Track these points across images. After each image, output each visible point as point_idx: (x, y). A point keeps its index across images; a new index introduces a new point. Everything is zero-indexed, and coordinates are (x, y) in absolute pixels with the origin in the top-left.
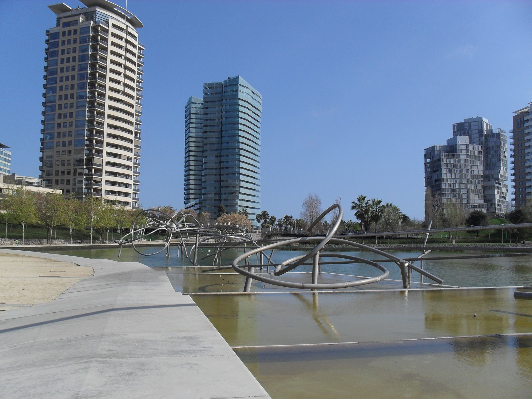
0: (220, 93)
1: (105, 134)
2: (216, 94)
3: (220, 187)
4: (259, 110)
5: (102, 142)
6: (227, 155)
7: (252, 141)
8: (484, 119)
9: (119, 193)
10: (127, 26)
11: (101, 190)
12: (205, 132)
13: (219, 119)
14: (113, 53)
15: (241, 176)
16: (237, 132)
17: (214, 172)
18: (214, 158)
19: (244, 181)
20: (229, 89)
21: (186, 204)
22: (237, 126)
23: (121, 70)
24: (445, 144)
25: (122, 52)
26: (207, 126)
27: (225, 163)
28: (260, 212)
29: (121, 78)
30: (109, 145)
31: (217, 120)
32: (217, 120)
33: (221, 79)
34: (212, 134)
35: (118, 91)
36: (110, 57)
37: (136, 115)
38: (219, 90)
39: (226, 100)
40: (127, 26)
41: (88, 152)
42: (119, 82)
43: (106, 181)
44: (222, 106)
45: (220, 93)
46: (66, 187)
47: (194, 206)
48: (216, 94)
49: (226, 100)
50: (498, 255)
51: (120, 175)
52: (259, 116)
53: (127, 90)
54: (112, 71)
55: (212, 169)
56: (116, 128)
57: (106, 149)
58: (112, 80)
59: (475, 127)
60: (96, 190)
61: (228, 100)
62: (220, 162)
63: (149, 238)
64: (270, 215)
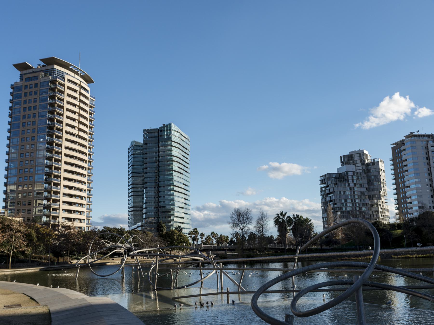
6: (164, 186)
10: (80, 81)
13: (156, 153)
24: (348, 154)
27: (162, 188)
30: (65, 179)
36: (67, 106)
38: (156, 134)
40: (80, 81)
48: (154, 137)
56: (72, 164)
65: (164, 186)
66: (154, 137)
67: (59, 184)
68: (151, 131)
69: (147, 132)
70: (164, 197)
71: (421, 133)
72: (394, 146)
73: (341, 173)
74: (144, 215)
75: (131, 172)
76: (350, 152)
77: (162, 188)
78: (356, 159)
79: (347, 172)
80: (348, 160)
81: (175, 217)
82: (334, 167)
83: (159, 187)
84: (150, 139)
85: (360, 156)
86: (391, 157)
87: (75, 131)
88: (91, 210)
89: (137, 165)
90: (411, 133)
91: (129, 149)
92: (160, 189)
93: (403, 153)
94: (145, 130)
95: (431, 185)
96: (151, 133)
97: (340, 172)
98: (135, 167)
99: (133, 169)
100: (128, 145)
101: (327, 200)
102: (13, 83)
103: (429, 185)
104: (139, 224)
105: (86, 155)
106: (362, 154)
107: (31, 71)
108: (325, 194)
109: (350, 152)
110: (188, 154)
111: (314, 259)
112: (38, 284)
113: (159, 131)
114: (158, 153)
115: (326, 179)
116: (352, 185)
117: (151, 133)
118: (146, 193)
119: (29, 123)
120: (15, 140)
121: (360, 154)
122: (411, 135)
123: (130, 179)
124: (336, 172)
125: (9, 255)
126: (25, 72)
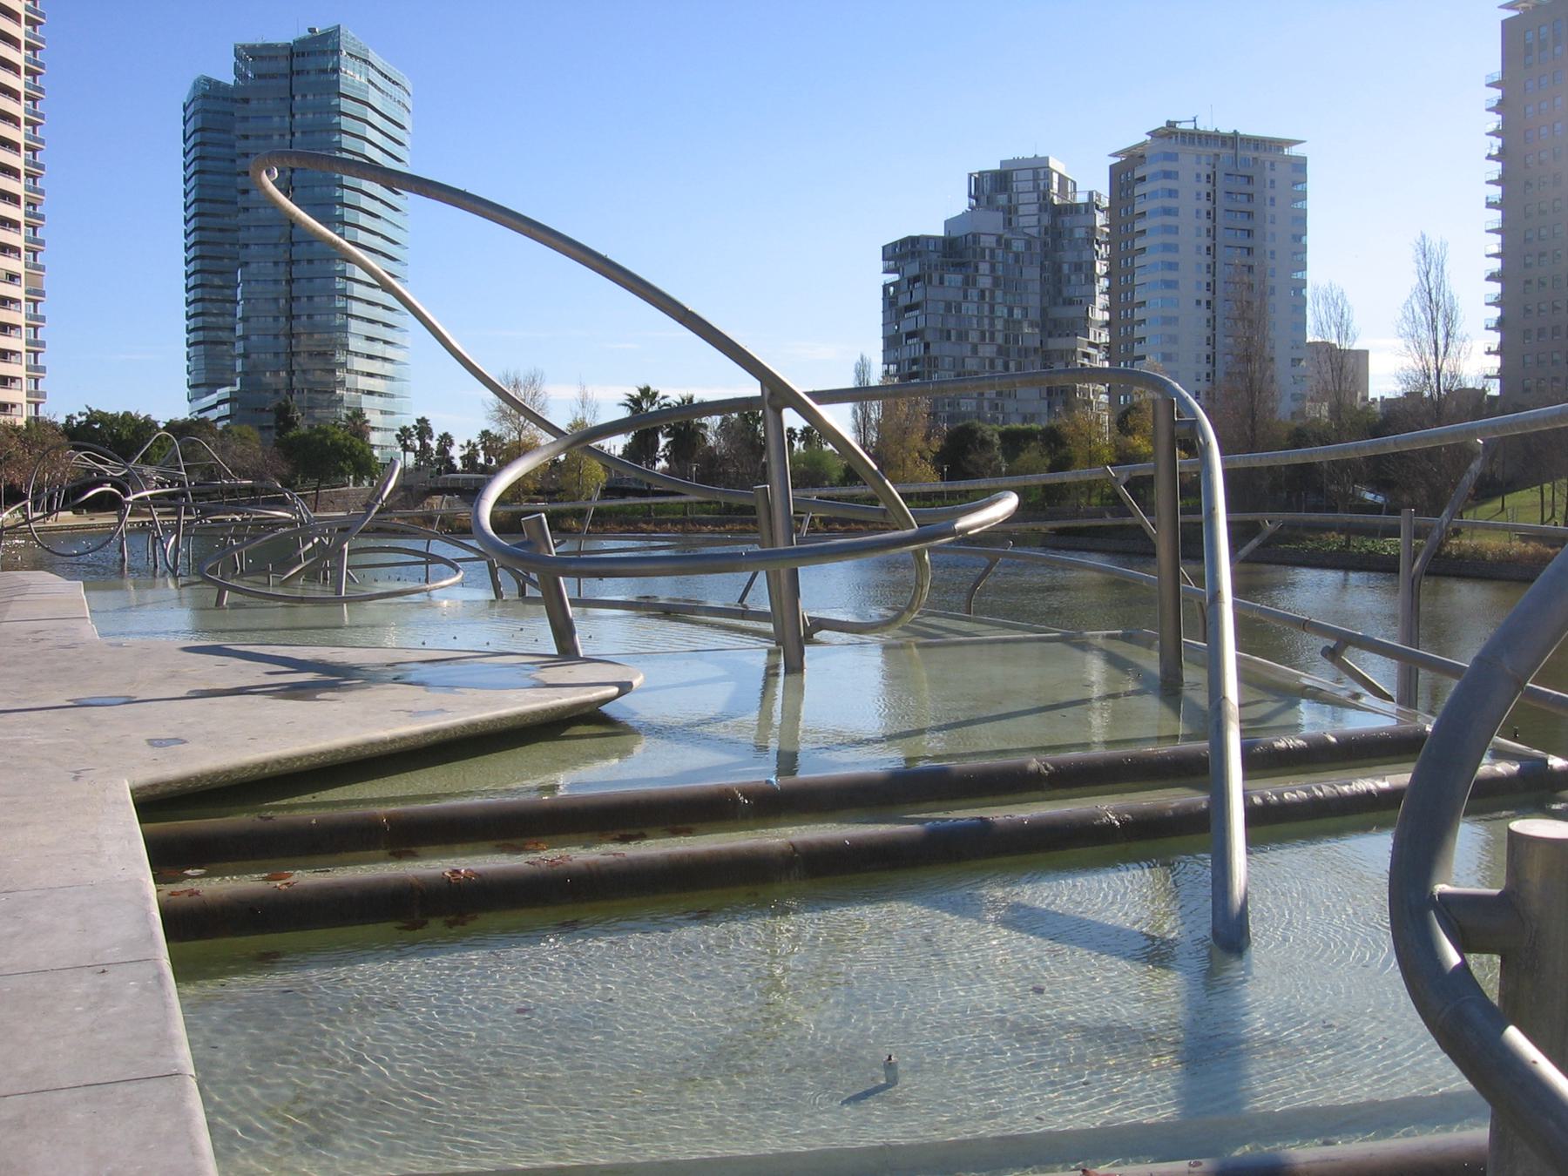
4: (402, 127)
6: (310, 261)
7: (382, 202)
8: (1053, 164)
13: (282, 136)
16: (337, 119)
19: (362, 319)
20: (310, 64)
22: (337, 138)
24: (997, 167)
27: (304, 265)
28: (410, 422)
31: (276, 137)
32: (276, 137)
33: (285, 32)
37: (28, 122)
39: (304, 96)
44: (293, 116)
47: (214, 407)
49: (304, 96)
52: (401, 144)
59: (1022, 183)
61: (310, 97)
63: (77, 509)
64: (437, 432)
65: (310, 261)
66: (273, 77)
68: (264, 53)
69: (250, 55)
70: (310, 298)
71: (1206, 125)
72: (1118, 160)
73: (955, 239)
74: (239, 363)
75: (192, 197)
76: (1002, 163)
77: (304, 265)
78: (1022, 186)
79: (974, 236)
81: (349, 371)
82: (936, 207)
83: (291, 262)
85: (1036, 179)
86: (1495, 67)
88: (43, 319)
89: (218, 173)
90: (1171, 124)
91: (185, 109)
92: (297, 271)
93: (1138, 190)
94: (243, 47)
95: (1208, 303)
96: (262, 58)
97: (954, 234)
98: (208, 177)
99: (199, 185)
100: (183, 93)
103: (1204, 304)
104: (224, 392)
105: (18, 125)
106: (1042, 172)
108: (894, 305)
109: (1002, 163)
110: (401, 144)
111: (853, 526)
113: (292, 55)
114: (288, 137)
115: (902, 253)
116: (985, 282)
117: (262, 58)
118: (246, 281)
121: (1035, 171)
122: (1169, 133)
123: (192, 183)
124: (939, 232)
125: (1263, 556)
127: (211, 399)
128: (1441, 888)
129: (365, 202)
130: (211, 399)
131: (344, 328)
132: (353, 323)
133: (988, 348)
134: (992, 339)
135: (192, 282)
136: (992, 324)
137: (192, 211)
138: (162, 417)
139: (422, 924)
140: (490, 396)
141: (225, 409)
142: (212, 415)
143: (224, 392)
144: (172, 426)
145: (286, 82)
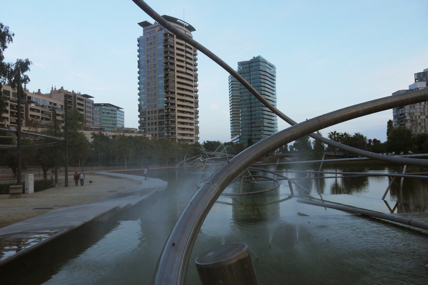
0: (248, 68)
1: (176, 117)
2: (246, 68)
3: (251, 127)
5: (174, 104)
6: (255, 107)
9: (187, 123)
10: (185, 31)
11: (175, 133)
12: (241, 93)
14: (178, 60)
15: (265, 120)
17: (247, 118)
18: (247, 109)
21: (232, 138)
23: (183, 59)
24: (423, 71)
25: (183, 59)
26: (241, 89)
27: (254, 108)
29: (183, 64)
30: (179, 105)
34: (244, 94)
35: (182, 73)
36: (176, 51)
38: (248, 66)
40: (185, 31)
41: (166, 111)
42: (182, 67)
43: (178, 128)
45: (248, 68)
46: (154, 132)
48: (246, 68)
50: (210, 254)
51: (187, 112)
53: (188, 71)
54: (178, 60)
55: (246, 116)
56: (183, 95)
57: (178, 120)
58: (178, 66)
60: (172, 121)
62: (251, 111)
65: (255, 107)
67: (175, 110)
75: (231, 95)
77: (254, 108)
80: (423, 77)
84: (244, 70)
87: (184, 70)
91: (229, 77)
96: (244, 64)
101: (398, 114)
102: (139, 37)
107: (150, 27)
109: (424, 70)
112: (402, 153)
117: (244, 64)
119: (151, 66)
120: (143, 57)
126: (146, 28)
127: (235, 138)
128: (131, 120)
129: (267, 93)
130: (235, 138)
131: (263, 122)
132: (265, 120)
133: (423, 117)
134: (424, 114)
135: (231, 113)
136: (424, 110)
137: (231, 98)
138: (223, 141)
139: (368, 183)
140: (228, 74)
141: (238, 140)
142: (234, 142)
143: (238, 136)
144: (226, 144)
145: (248, 69)
